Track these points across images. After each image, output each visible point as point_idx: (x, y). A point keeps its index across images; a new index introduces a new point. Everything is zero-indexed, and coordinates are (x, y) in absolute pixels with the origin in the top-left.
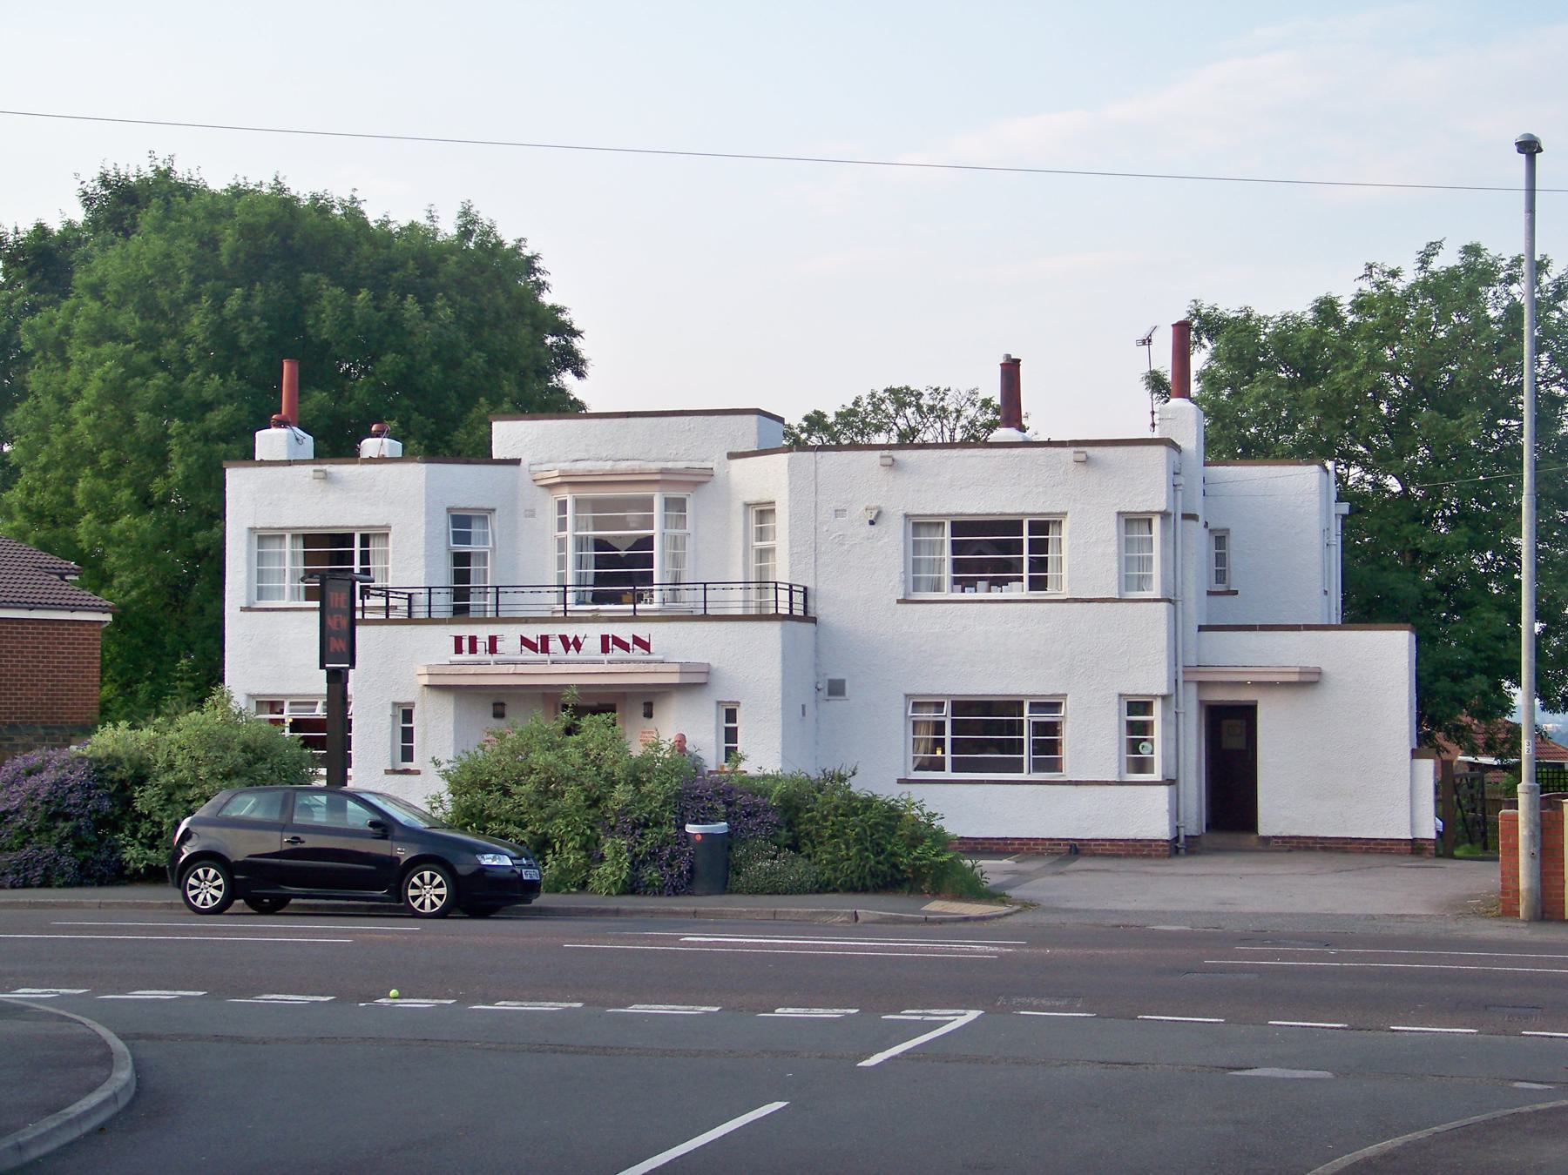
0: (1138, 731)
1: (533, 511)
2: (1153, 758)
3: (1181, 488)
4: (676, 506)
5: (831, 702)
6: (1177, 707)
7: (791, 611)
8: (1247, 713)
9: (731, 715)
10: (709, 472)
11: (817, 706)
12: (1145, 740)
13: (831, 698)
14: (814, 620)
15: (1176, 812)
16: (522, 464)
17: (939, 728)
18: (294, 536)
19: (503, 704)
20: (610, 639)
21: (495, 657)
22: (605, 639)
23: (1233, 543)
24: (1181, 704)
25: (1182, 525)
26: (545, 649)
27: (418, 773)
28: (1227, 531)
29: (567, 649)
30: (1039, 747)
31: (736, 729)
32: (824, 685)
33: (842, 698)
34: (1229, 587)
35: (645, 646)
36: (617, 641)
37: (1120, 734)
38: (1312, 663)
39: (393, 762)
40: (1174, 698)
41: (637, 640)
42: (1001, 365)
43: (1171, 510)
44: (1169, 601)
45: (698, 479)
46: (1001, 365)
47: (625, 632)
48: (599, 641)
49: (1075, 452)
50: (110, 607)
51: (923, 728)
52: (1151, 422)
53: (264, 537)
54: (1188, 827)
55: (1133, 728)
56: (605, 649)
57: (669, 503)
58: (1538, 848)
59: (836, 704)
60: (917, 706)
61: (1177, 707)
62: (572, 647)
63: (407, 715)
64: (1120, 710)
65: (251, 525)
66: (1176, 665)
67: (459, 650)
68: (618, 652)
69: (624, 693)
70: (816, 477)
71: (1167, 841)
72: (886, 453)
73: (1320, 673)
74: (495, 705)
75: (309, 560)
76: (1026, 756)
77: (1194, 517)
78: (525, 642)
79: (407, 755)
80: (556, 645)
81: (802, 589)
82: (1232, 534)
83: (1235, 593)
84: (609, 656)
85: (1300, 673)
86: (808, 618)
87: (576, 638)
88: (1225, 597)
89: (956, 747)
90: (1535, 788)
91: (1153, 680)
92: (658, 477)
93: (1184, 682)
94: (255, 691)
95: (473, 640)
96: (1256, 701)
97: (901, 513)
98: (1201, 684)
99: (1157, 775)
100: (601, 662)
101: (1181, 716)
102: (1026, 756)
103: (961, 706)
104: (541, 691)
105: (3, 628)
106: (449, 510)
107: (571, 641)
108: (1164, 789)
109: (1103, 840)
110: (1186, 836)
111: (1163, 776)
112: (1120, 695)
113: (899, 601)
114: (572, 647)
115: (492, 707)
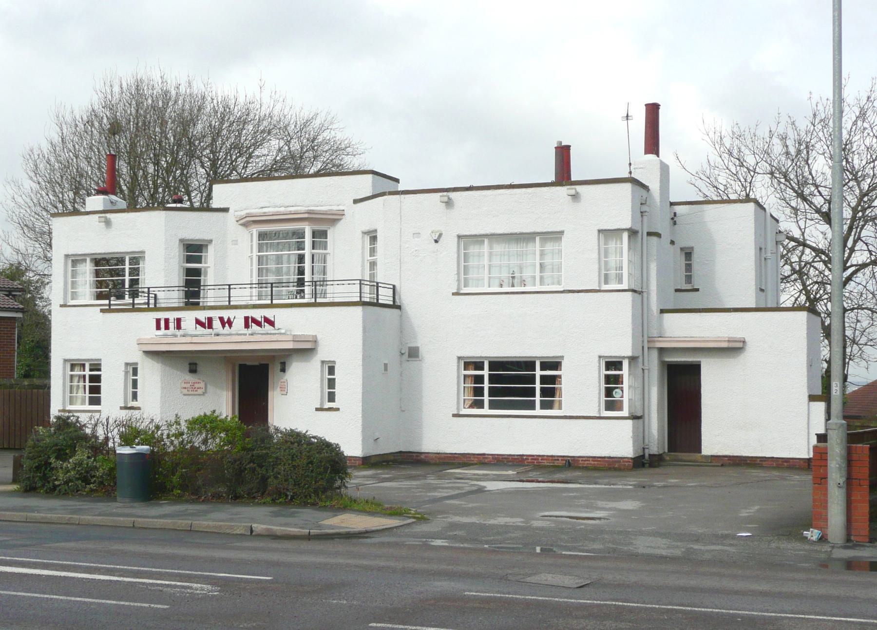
0: (612, 382)
1: (237, 241)
2: (623, 400)
3: (646, 214)
4: (320, 236)
5: (411, 362)
6: (643, 365)
7: (378, 300)
8: (695, 369)
9: (331, 370)
10: (341, 213)
11: (401, 364)
12: (617, 388)
13: (409, 359)
14: (399, 307)
15: (640, 436)
16: (230, 211)
17: (479, 379)
18: (92, 260)
19: (196, 364)
20: (250, 319)
21: (181, 332)
22: (246, 319)
23: (695, 256)
24: (646, 364)
25: (647, 241)
26: (210, 326)
27: (338, 409)
28: (692, 248)
29: (223, 326)
30: (545, 392)
31: (334, 379)
32: (405, 350)
33: (417, 359)
34: (693, 286)
35: (271, 323)
36: (255, 321)
37: (600, 382)
38: (739, 335)
39: (126, 401)
40: (641, 359)
41: (267, 320)
42: (555, 148)
43: (637, 227)
44: (634, 291)
45: (333, 219)
46: (555, 148)
47: (258, 314)
48: (243, 320)
49: (567, 189)
50: (21, 309)
51: (469, 380)
52: (629, 171)
53: (75, 260)
54: (651, 448)
55: (608, 379)
56: (247, 326)
57: (314, 234)
58: (844, 479)
59: (413, 364)
60: (467, 365)
61: (643, 365)
62: (227, 325)
63: (135, 372)
64: (599, 367)
65: (66, 253)
66: (643, 336)
67: (158, 327)
68: (255, 327)
69: (274, 356)
70: (401, 212)
71: (631, 458)
72: (445, 194)
73: (744, 342)
74: (190, 364)
75: (97, 273)
76: (538, 398)
77: (658, 235)
78: (198, 322)
79: (332, 398)
80: (217, 324)
81: (392, 287)
82: (695, 250)
83: (697, 290)
84: (250, 331)
85: (729, 341)
86: (395, 306)
87: (229, 319)
88: (691, 293)
89: (492, 392)
90: (842, 425)
91: (623, 347)
92: (306, 216)
93: (648, 348)
94: (68, 357)
95: (167, 321)
96: (700, 362)
97: (455, 234)
98: (661, 350)
99: (625, 413)
100: (245, 335)
101: (646, 372)
102: (538, 398)
103: (495, 365)
104: (223, 355)
105: (2, 325)
106: (181, 240)
107: (226, 320)
108: (630, 422)
109: (587, 457)
110: (650, 455)
111: (629, 413)
112: (600, 357)
113: (453, 294)
114: (227, 325)
115: (188, 366)
